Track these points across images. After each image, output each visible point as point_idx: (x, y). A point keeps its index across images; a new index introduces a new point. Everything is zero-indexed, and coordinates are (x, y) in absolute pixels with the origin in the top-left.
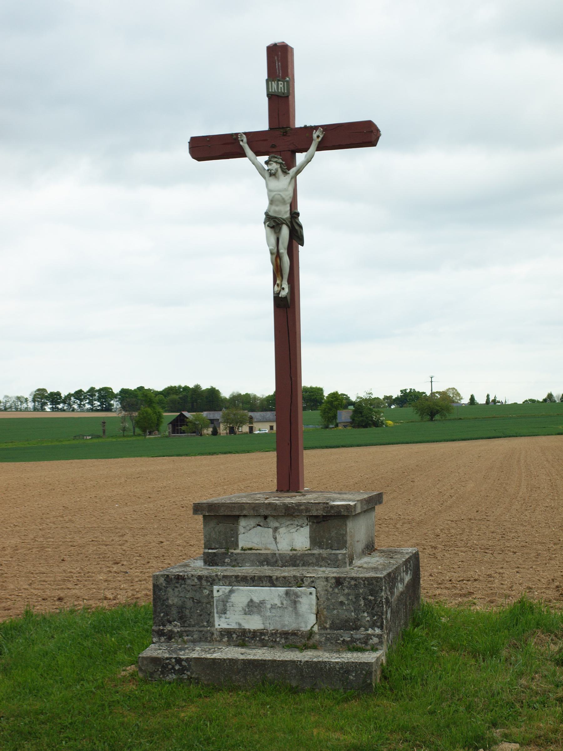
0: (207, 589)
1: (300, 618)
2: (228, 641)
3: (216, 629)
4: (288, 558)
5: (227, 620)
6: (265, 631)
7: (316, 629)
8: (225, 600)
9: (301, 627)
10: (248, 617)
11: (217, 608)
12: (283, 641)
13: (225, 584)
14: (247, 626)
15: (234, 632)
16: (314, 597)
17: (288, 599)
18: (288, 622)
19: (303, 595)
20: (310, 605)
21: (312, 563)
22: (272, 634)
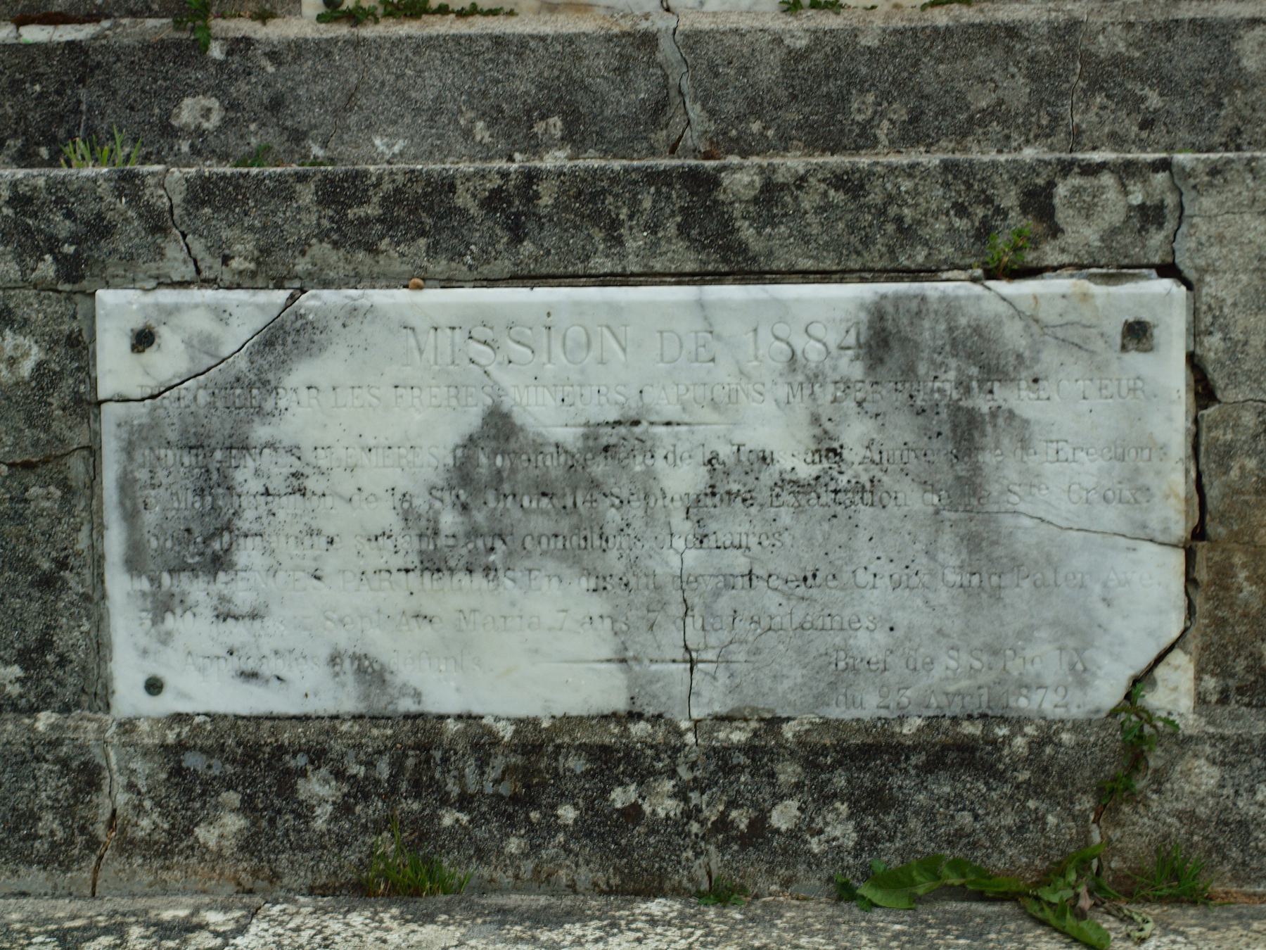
0: (23, 326)
1: (1019, 593)
2: (248, 845)
3: (128, 726)
4: (767, 73)
5: (237, 632)
6: (639, 729)
7: (1175, 694)
8: (219, 425)
9: (1024, 686)
10: (461, 592)
11: (131, 517)
12: (840, 828)
13: (211, 266)
14: (444, 690)
15: (318, 756)
16: (1168, 370)
17: (887, 396)
18: (890, 636)
19: (1050, 356)
20: (1129, 451)
21: (990, 114)
22: (722, 758)
